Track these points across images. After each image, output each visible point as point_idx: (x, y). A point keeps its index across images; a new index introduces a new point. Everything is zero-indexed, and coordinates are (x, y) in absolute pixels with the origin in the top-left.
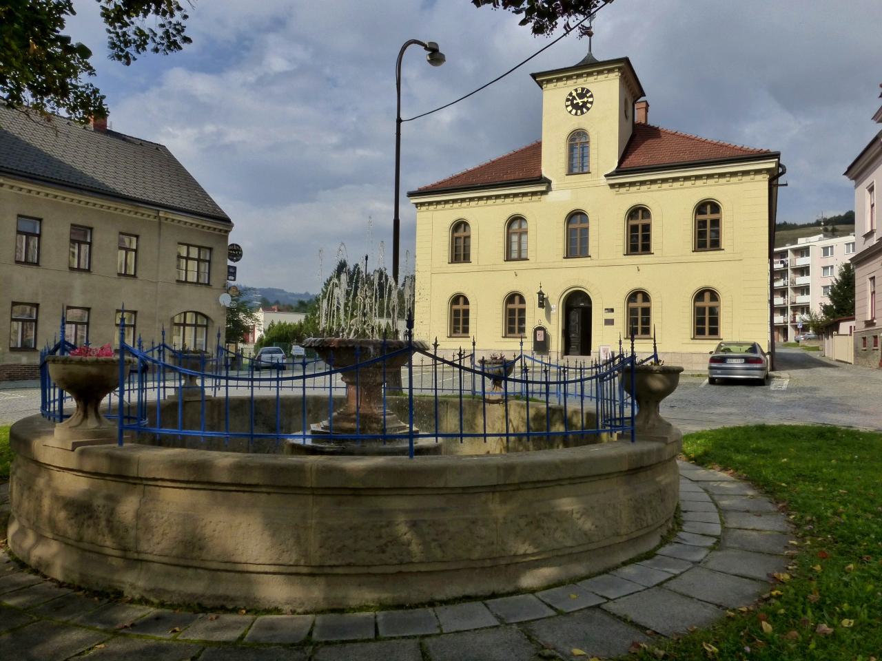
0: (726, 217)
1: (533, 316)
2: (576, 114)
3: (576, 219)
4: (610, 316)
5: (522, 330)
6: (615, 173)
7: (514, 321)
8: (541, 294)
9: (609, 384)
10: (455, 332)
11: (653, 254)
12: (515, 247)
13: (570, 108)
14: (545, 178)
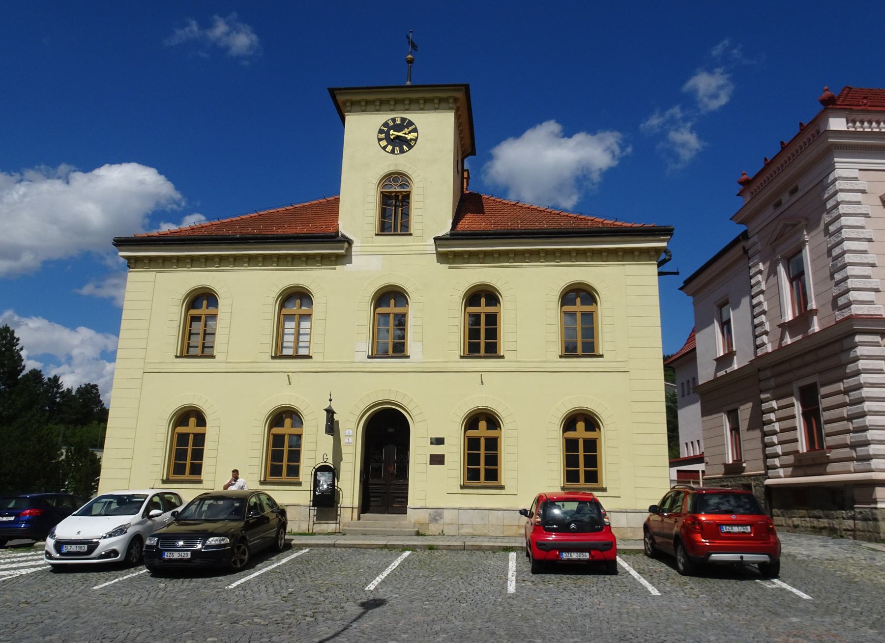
0: (506, 313)
1: (315, 449)
2: (393, 152)
3: (390, 297)
4: (437, 450)
5: (294, 471)
6: (449, 236)
7: (282, 458)
8: (330, 412)
9: (42, 562)
10: (273, 473)
11: (503, 357)
12: (289, 339)
13: (384, 143)
14: (343, 236)
